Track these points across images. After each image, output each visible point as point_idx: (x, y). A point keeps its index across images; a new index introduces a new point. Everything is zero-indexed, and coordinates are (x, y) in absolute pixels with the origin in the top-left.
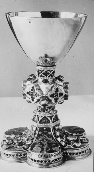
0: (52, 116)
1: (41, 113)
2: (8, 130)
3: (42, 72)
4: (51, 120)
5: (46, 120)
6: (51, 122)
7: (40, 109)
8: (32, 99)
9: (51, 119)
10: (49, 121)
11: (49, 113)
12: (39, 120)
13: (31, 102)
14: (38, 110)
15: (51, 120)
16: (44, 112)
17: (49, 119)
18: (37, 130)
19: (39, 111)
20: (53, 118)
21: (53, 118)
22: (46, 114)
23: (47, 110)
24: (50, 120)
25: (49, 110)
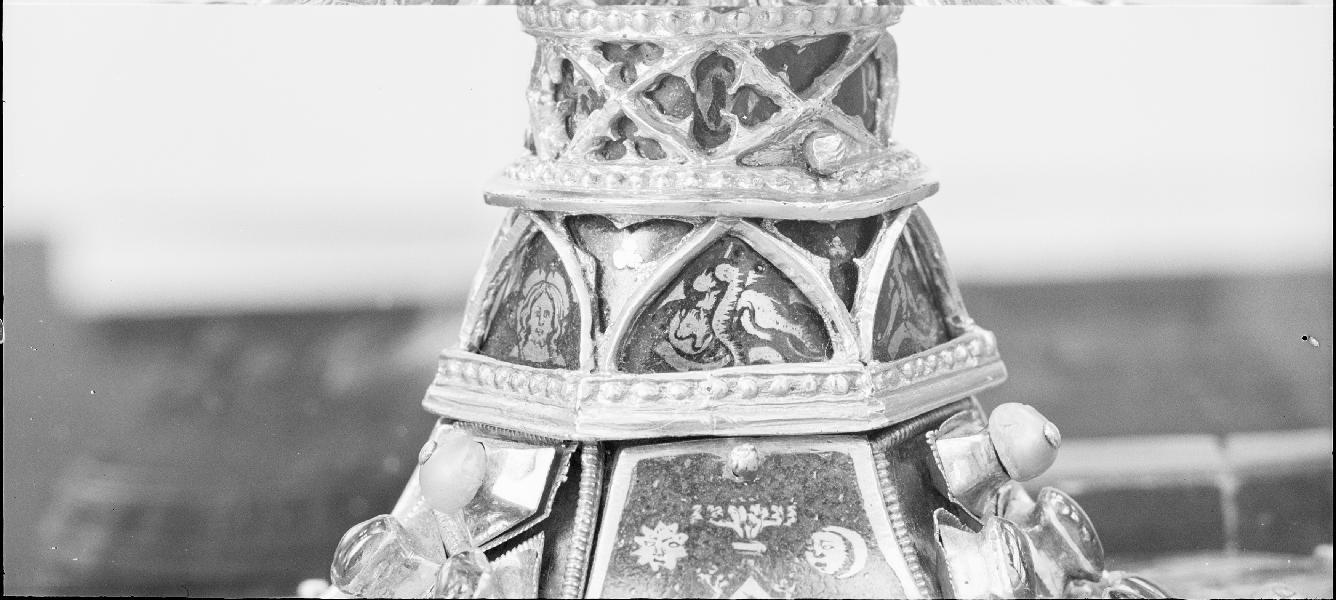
0: (865, 231)
1: (658, 169)
2: (508, 553)
3: (624, 74)
4: (849, 299)
5: (751, 298)
6: (855, 335)
7: (620, 101)
8: (575, 300)
9: (847, 281)
10: (811, 316)
11: (800, 159)
12: (621, 311)
13: (510, 176)
14: (593, 125)
15: (849, 299)
16: (706, 135)
17: (811, 272)
18: (532, 300)
19: (606, 149)
20: (874, 268)
21: (874, 268)
22: (745, 180)
23: (768, 106)
24: (829, 303)
25: (793, 107)
